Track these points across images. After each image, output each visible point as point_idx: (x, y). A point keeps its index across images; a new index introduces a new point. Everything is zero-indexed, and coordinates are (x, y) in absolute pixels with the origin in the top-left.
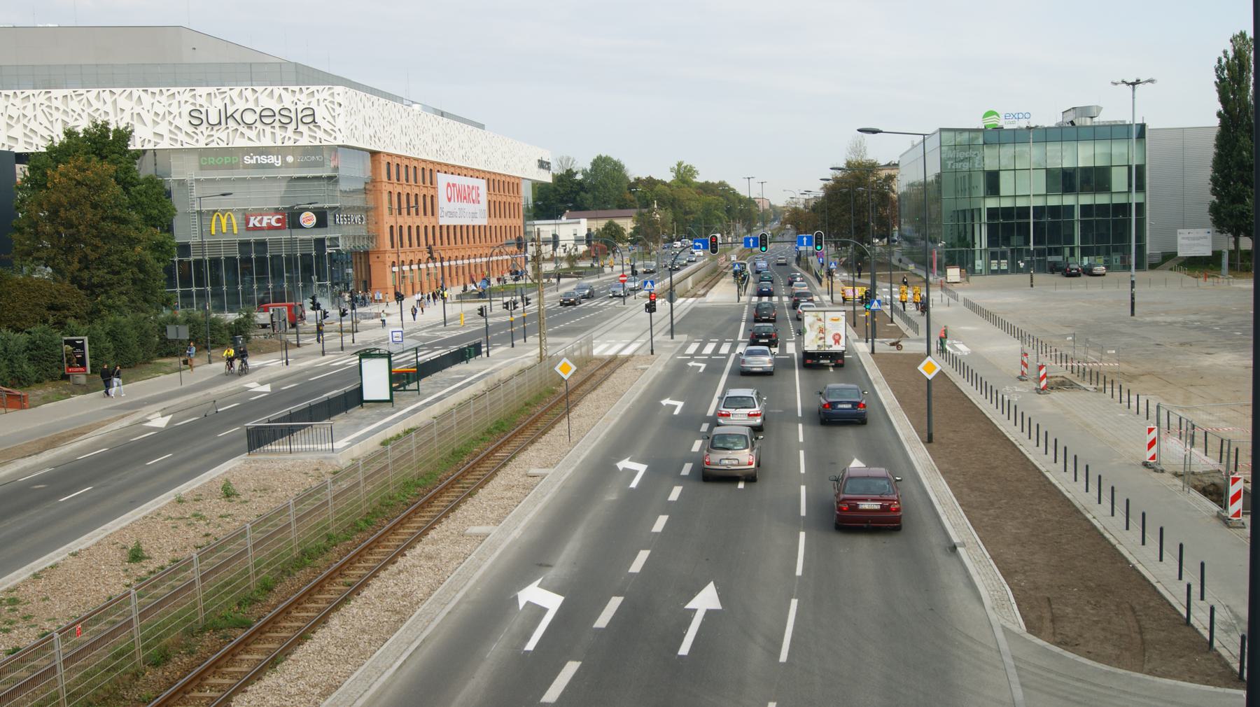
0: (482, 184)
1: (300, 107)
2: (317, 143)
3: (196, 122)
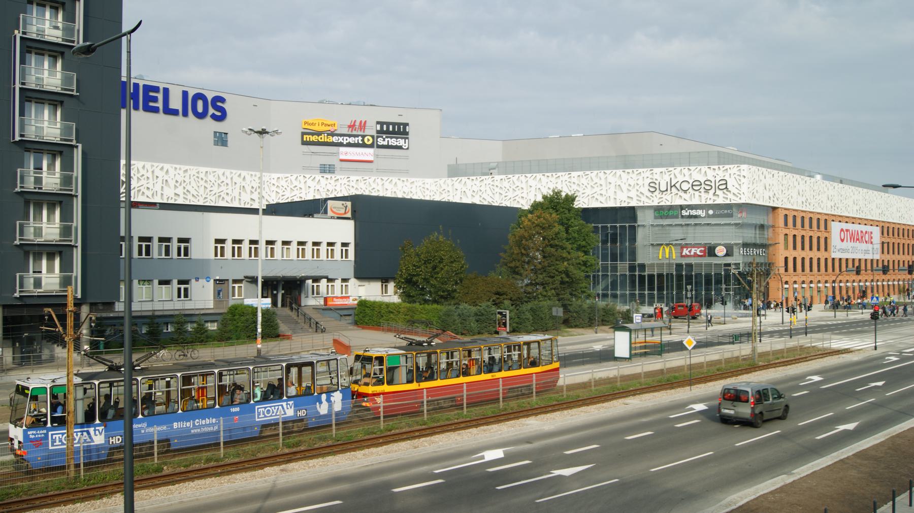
0: (876, 231)
1: (718, 179)
2: (728, 202)
3: (653, 190)
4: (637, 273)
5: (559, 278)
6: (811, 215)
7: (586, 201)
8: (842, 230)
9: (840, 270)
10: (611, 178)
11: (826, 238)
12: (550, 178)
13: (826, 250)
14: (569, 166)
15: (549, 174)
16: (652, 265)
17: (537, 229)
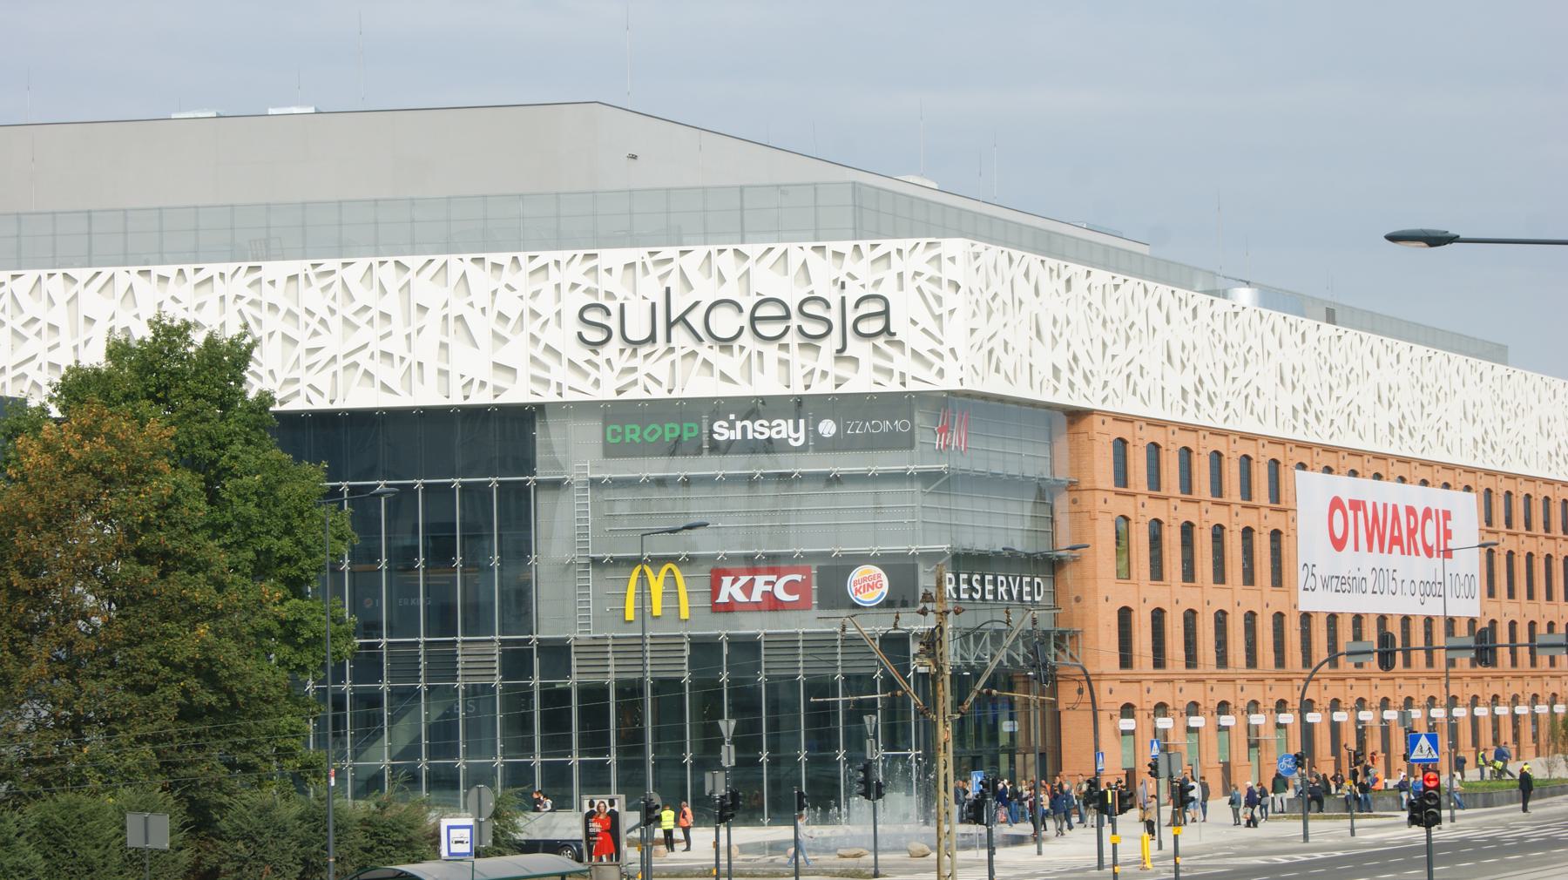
0: (1465, 511)
1: (852, 295)
2: (893, 386)
3: (595, 336)
4: (536, 681)
5: (173, 692)
6: (1220, 444)
7: (323, 381)
8: (1336, 503)
9: (1307, 661)
10: (426, 289)
11: (1276, 535)
12: (507, 276)
13: (1277, 580)
14: (251, 237)
15: (170, 270)
16: (597, 648)
17: (81, 483)
